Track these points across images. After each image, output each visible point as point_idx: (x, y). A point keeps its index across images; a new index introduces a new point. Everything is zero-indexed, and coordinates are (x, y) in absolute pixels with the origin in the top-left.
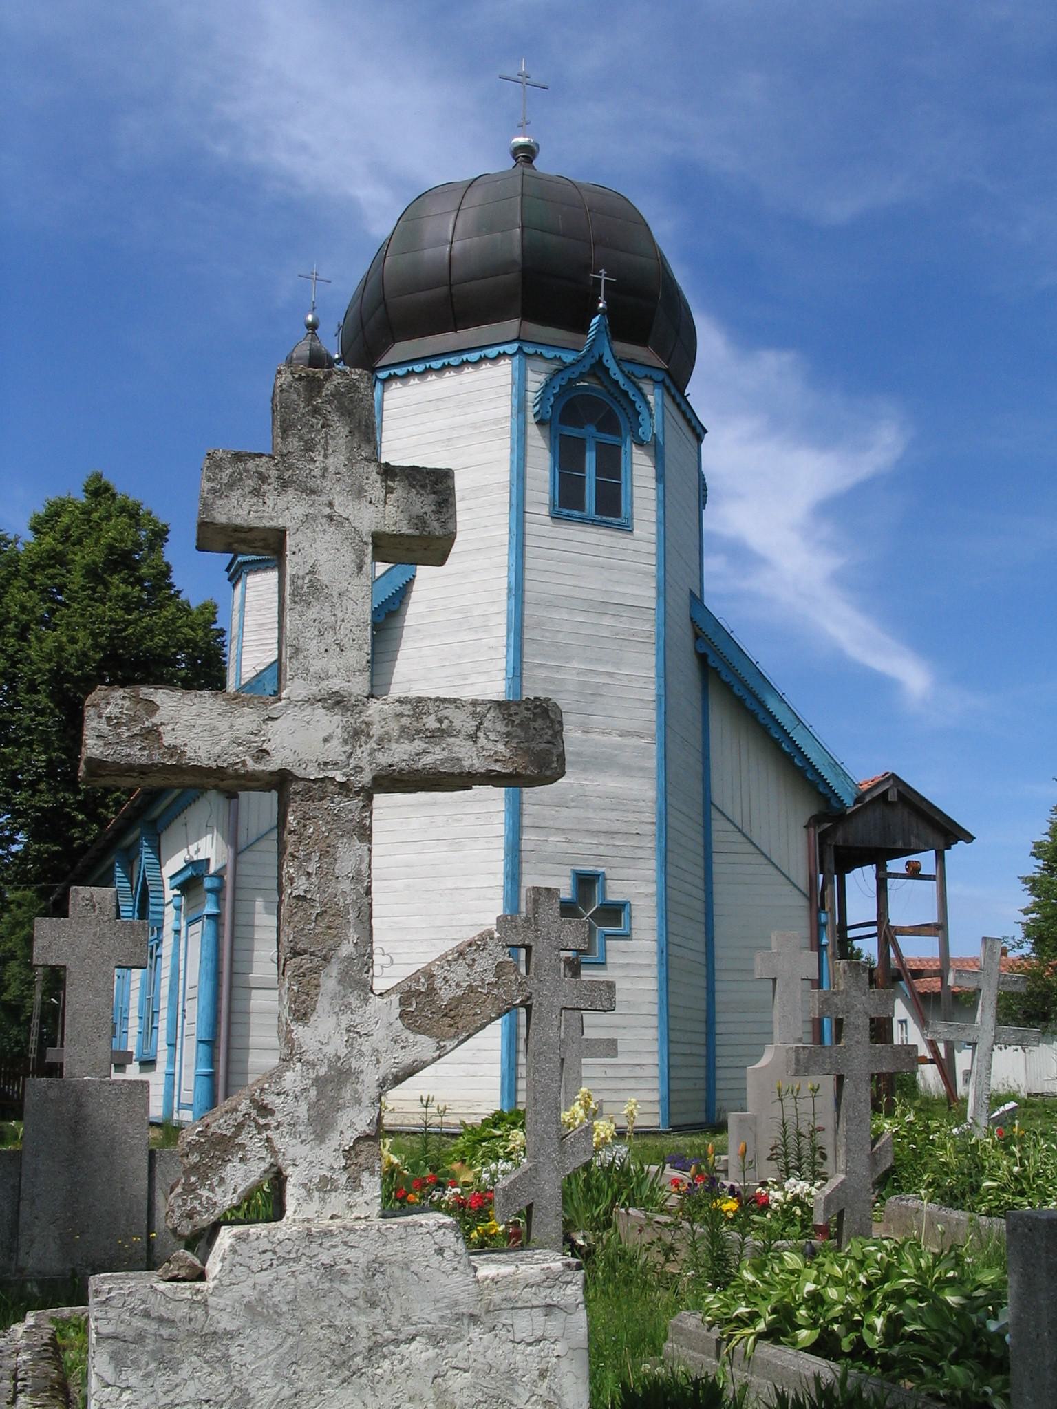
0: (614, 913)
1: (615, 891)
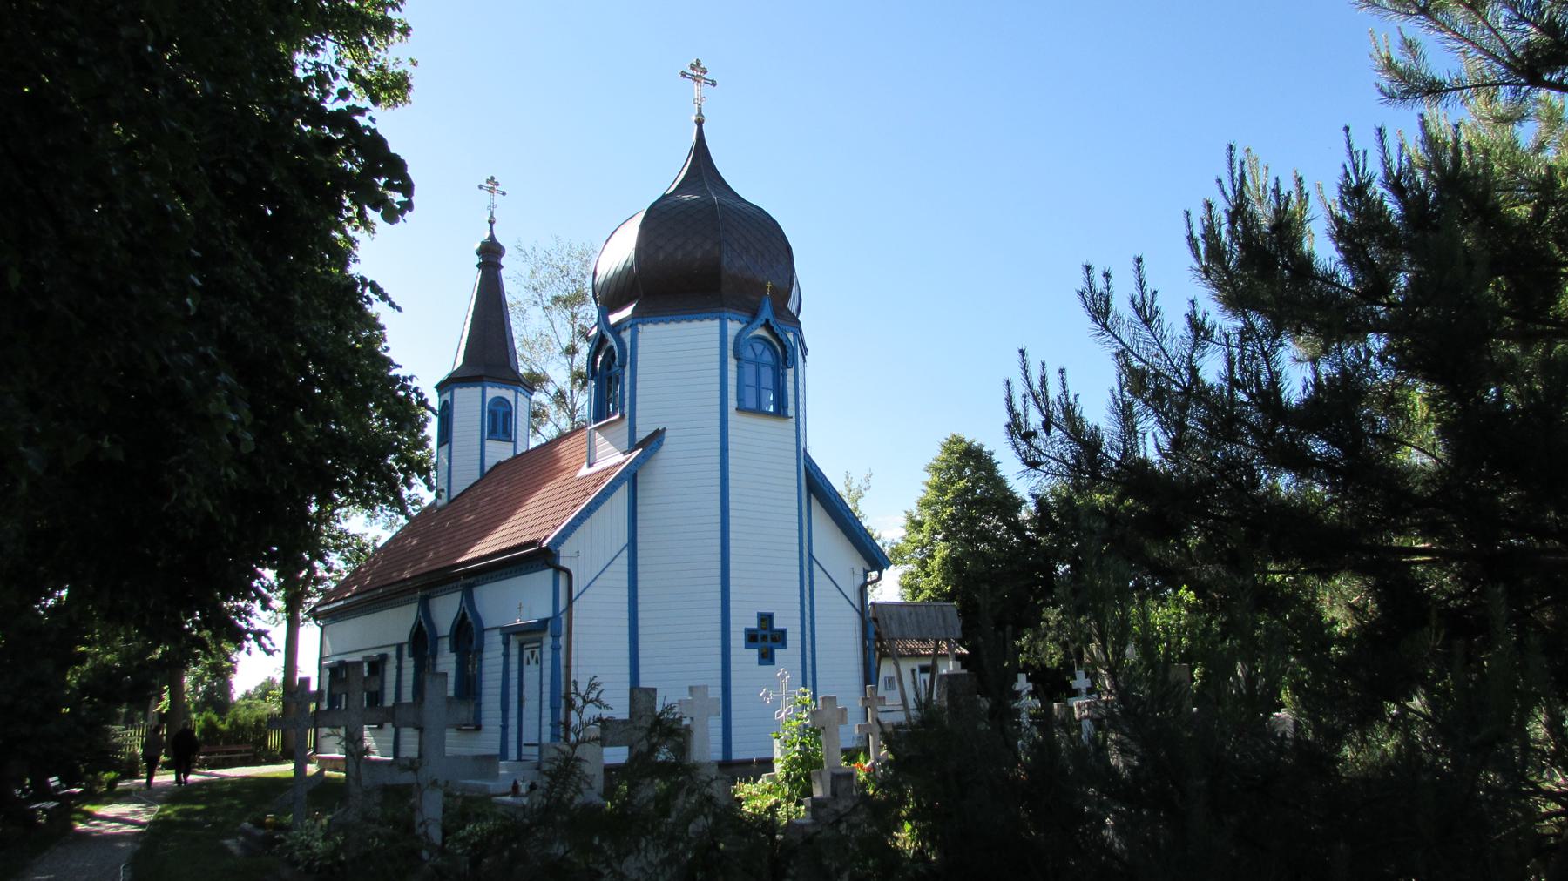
0: (780, 638)
1: (777, 625)
